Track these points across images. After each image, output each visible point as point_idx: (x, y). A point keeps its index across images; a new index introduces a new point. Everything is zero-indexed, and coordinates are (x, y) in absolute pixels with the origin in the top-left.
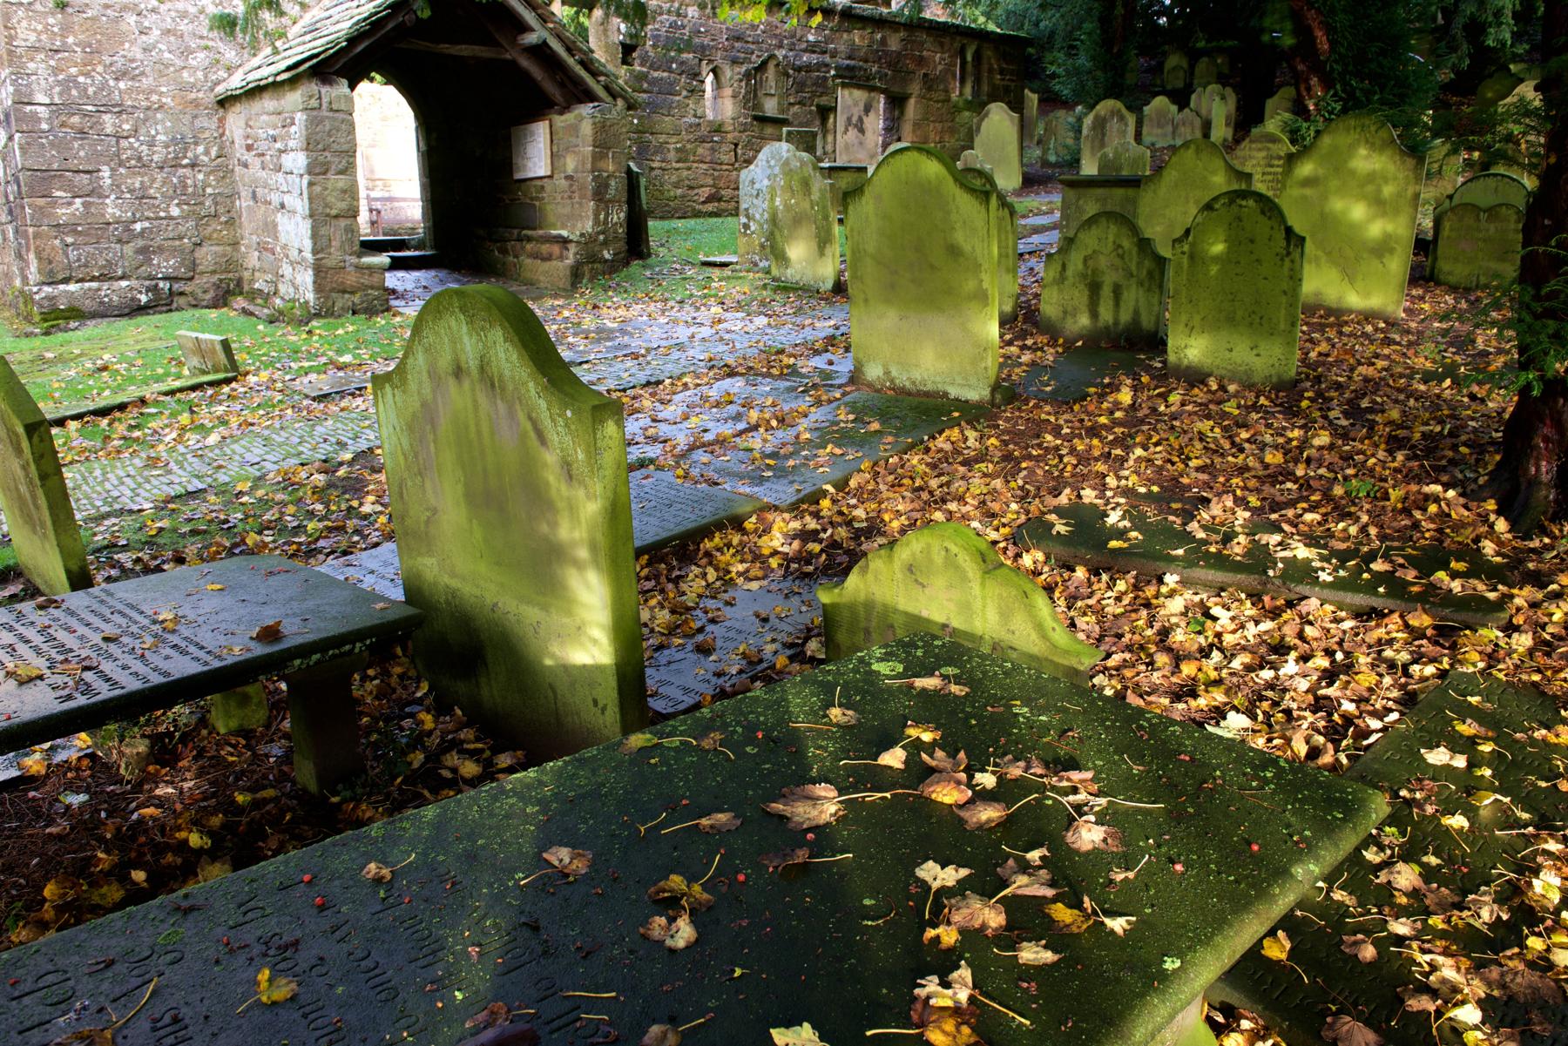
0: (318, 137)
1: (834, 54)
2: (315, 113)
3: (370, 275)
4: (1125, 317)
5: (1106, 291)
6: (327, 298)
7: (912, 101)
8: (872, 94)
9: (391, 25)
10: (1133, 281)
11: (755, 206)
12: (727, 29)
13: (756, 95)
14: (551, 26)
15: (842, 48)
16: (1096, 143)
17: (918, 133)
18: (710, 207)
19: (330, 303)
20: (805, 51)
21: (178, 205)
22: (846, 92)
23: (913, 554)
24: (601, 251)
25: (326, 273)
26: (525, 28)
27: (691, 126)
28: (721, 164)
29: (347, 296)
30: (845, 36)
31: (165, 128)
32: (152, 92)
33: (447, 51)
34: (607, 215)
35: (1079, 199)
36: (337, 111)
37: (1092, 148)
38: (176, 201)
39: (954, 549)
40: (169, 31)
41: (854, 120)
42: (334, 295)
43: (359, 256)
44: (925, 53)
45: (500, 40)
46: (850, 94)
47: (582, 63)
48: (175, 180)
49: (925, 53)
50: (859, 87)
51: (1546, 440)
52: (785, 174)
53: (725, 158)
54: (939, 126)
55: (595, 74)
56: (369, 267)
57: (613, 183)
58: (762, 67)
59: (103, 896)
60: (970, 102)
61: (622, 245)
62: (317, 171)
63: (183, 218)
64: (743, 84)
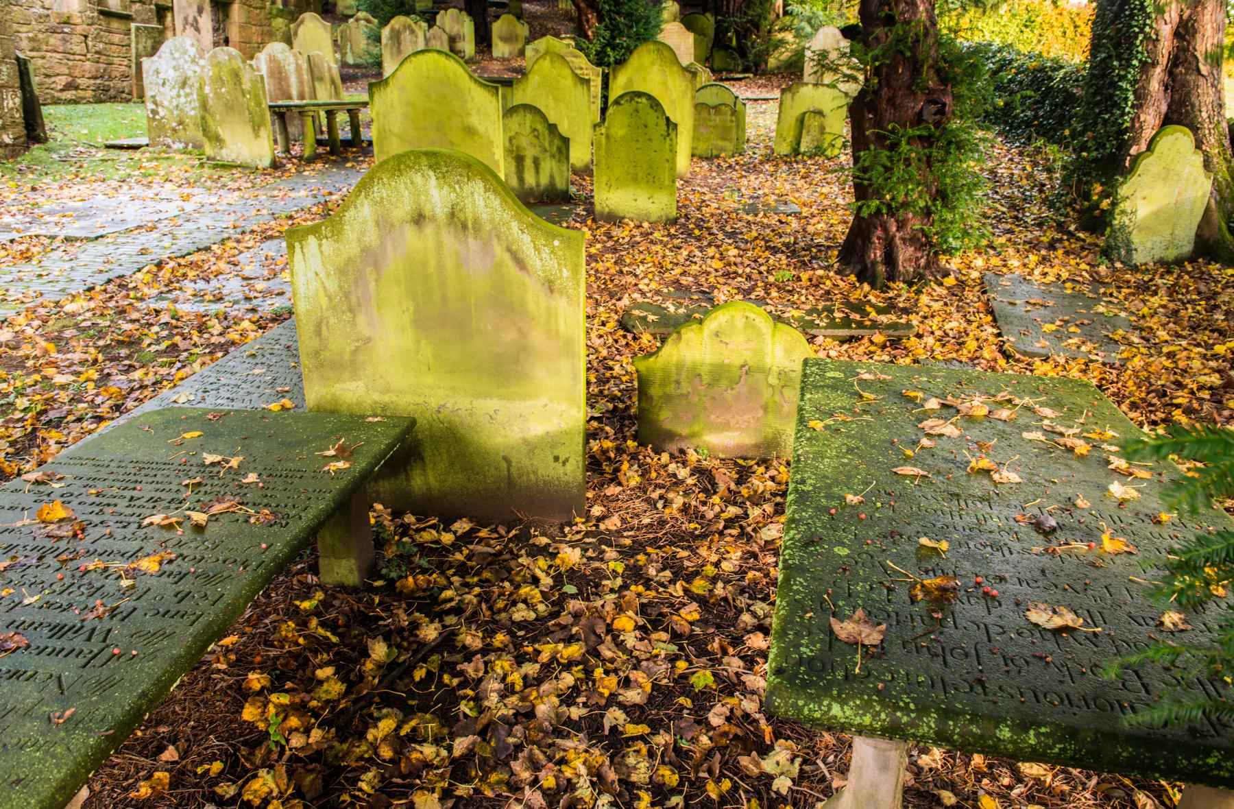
4: (544, 181)
5: (528, 163)
10: (548, 154)
11: (162, 94)
16: (395, 50)
18: (69, 95)
23: (720, 325)
27: (40, 17)
37: (392, 54)
39: (752, 316)
41: (190, 19)
51: (879, 238)
52: (212, 65)
59: (326, 692)
60: (281, 11)
61: (21, 130)
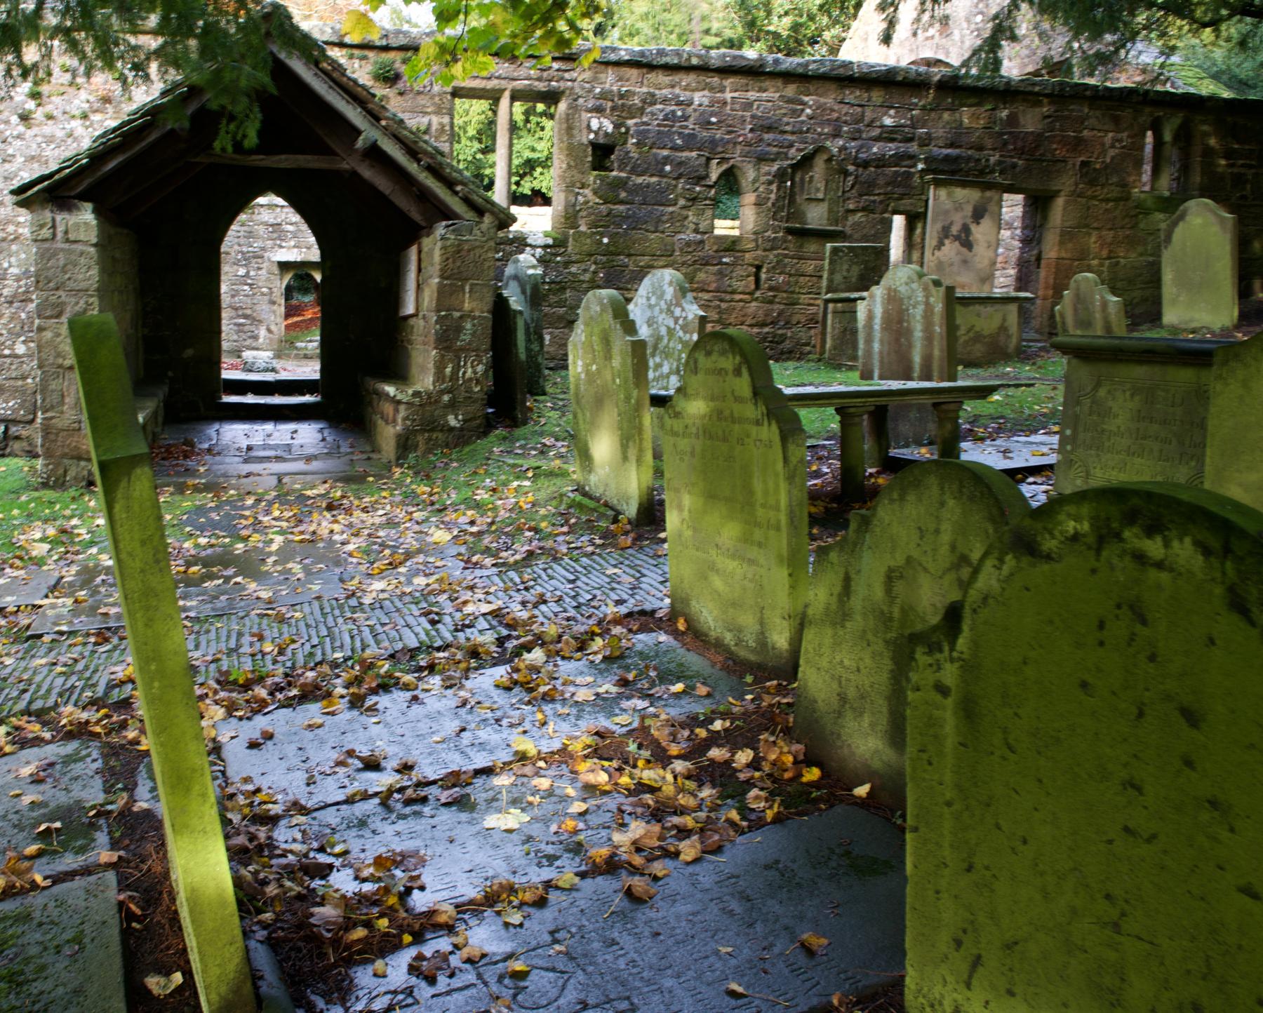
0: (50, 273)
1: (925, 142)
2: (47, 245)
6: (57, 465)
7: (1060, 202)
8: (988, 194)
12: (753, 117)
13: (792, 201)
15: (939, 132)
17: (1070, 245)
19: (61, 471)
20: (877, 139)
21: (24, 342)
22: (943, 193)
24: (446, 415)
25: (57, 435)
26: (358, 132)
27: (688, 244)
28: (733, 292)
30: (946, 116)
31: (19, 260)
32: (8, 222)
34: (457, 368)
35: (1098, 385)
36: (75, 242)
38: (23, 338)
40: (33, 158)
41: (955, 230)
42: (66, 461)
44: (1085, 133)
45: (333, 146)
46: (949, 195)
47: (431, 169)
48: (23, 316)
49: (1085, 133)
50: (964, 184)
53: (738, 285)
54: (1109, 235)
55: (450, 184)
57: (468, 326)
58: (806, 162)
62: (48, 313)
63: (29, 356)
64: (774, 187)
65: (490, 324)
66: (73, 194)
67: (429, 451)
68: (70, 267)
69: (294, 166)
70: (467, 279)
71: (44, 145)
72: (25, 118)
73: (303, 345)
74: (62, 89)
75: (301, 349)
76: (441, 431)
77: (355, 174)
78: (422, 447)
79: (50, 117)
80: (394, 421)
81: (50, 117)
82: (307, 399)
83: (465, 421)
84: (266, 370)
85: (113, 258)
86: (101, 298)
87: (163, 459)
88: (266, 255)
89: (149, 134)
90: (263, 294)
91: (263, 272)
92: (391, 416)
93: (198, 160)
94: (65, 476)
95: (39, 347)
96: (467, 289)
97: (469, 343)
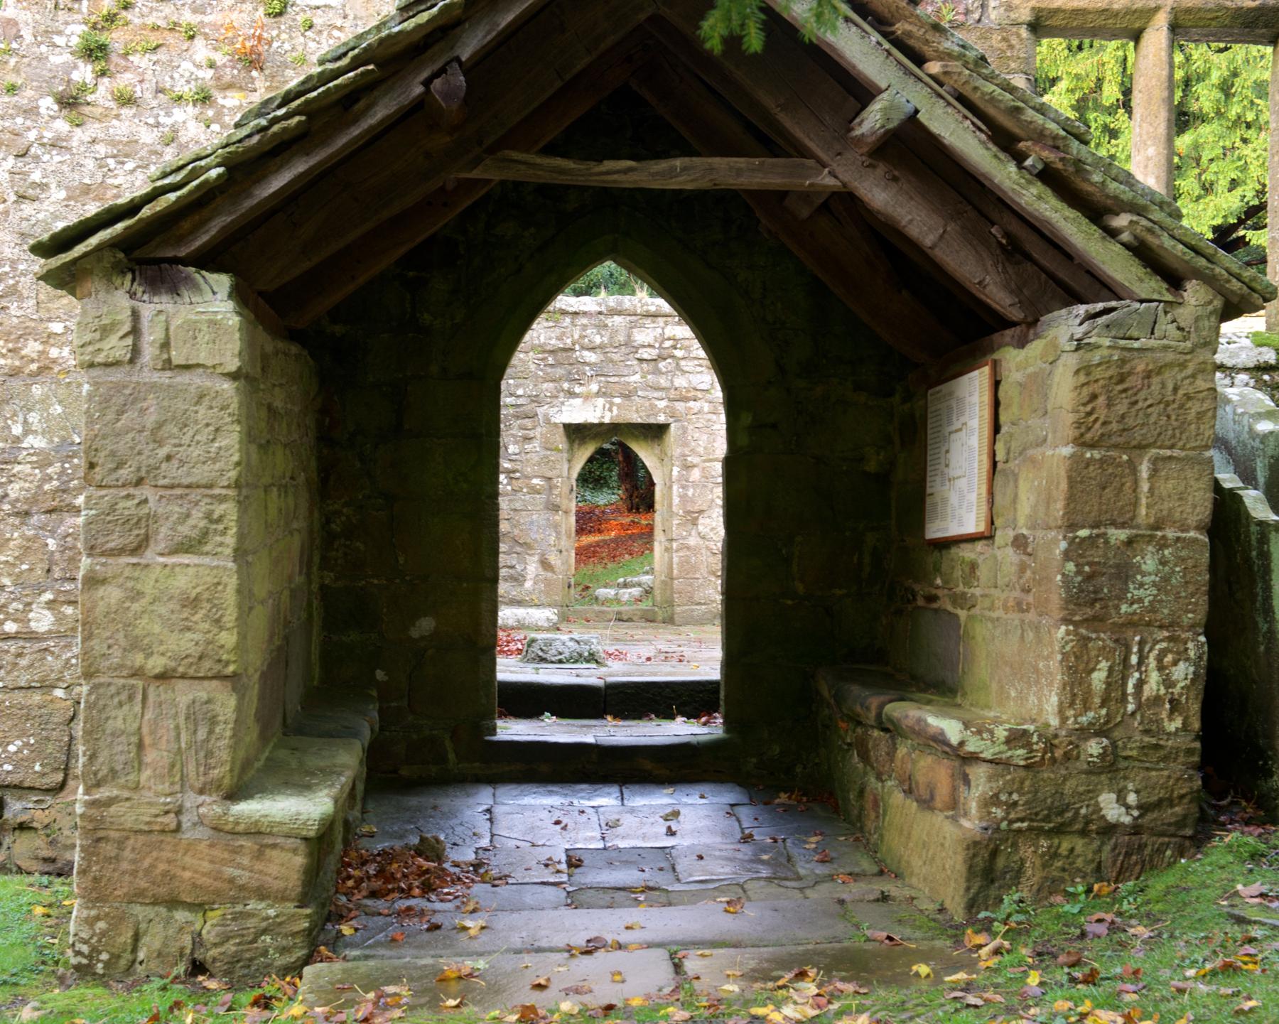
0: (122, 446)
2: (117, 375)
3: (259, 855)
6: (117, 921)
9: (381, 112)
14: (934, 67)
19: (126, 937)
21: (50, 605)
24: (1093, 793)
25: (121, 844)
26: (863, 93)
29: (181, 916)
31: (47, 419)
33: (628, 181)
36: (187, 367)
42: (138, 910)
43: (234, 795)
45: (799, 134)
47: (1049, 177)
48: (52, 544)
56: (256, 831)
57: (1150, 564)
62: (114, 542)
65: (1205, 557)
66: (183, 252)
67: (1051, 886)
68: (172, 428)
69: (704, 184)
70: (1142, 447)
71: (111, 162)
72: (70, 102)
73: (611, 592)
74: (154, 39)
75: (606, 601)
76: (1084, 833)
77: (847, 201)
78: (1033, 874)
79: (126, 100)
80: (954, 804)
81: (126, 100)
82: (679, 730)
83: (1144, 808)
84: (577, 658)
85: (270, 408)
86: (242, 504)
87: (373, 894)
88: (541, 411)
89: (369, 107)
90: (534, 491)
91: (536, 445)
92: (943, 791)
93: (475, 174)
94: (134, 950)
95: (88, 626)
96: (1144, 470)
97: (1152, 609)
